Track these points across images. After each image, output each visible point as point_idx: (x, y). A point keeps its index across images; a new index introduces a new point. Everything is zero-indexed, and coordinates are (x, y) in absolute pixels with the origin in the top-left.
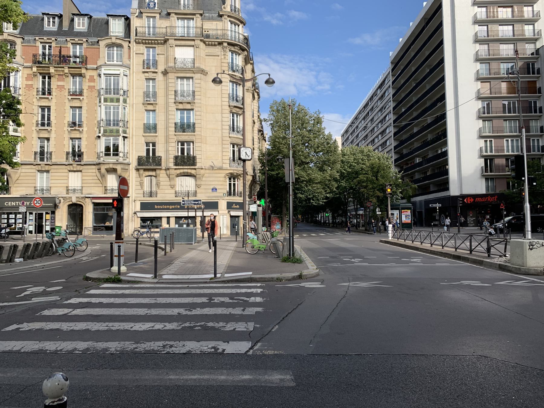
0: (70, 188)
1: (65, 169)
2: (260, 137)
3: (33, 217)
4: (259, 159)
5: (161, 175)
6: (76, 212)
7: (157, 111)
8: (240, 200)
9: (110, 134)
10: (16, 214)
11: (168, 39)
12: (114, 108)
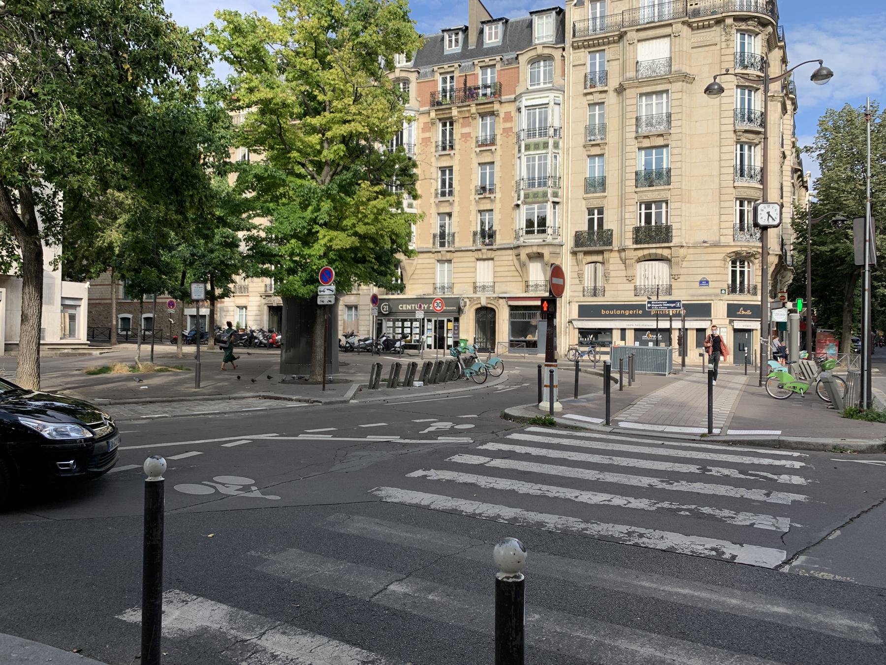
0: (478, 284)
1: (471, 256)
2: (796, 183)
3: (431, 326)
4: (793, 224)
5: (611, 261)
6: (486, 318)
7: (606, 156)
8: (757, 300)
9: (534, 200)
10: (412, 321)
11: (626, 33)
12: (540, 159)
